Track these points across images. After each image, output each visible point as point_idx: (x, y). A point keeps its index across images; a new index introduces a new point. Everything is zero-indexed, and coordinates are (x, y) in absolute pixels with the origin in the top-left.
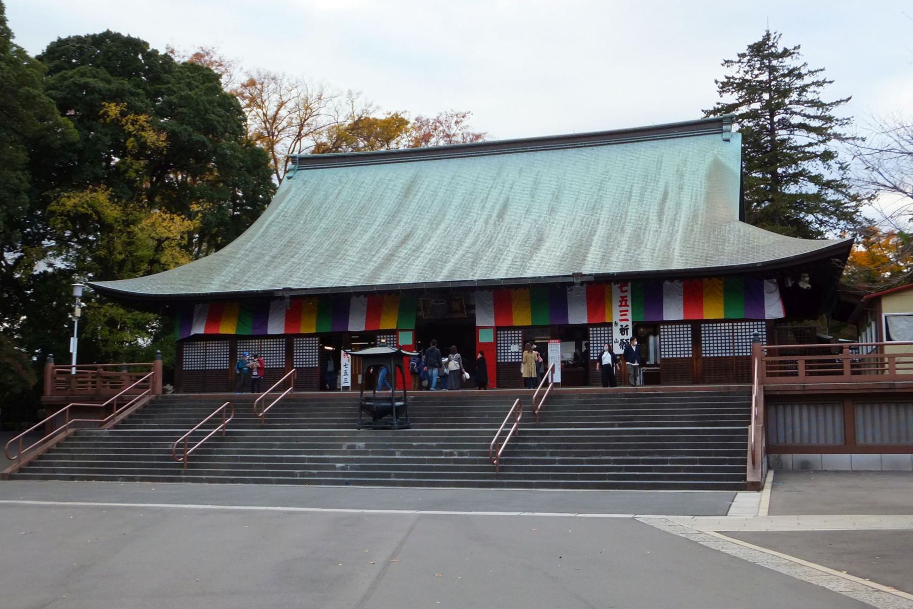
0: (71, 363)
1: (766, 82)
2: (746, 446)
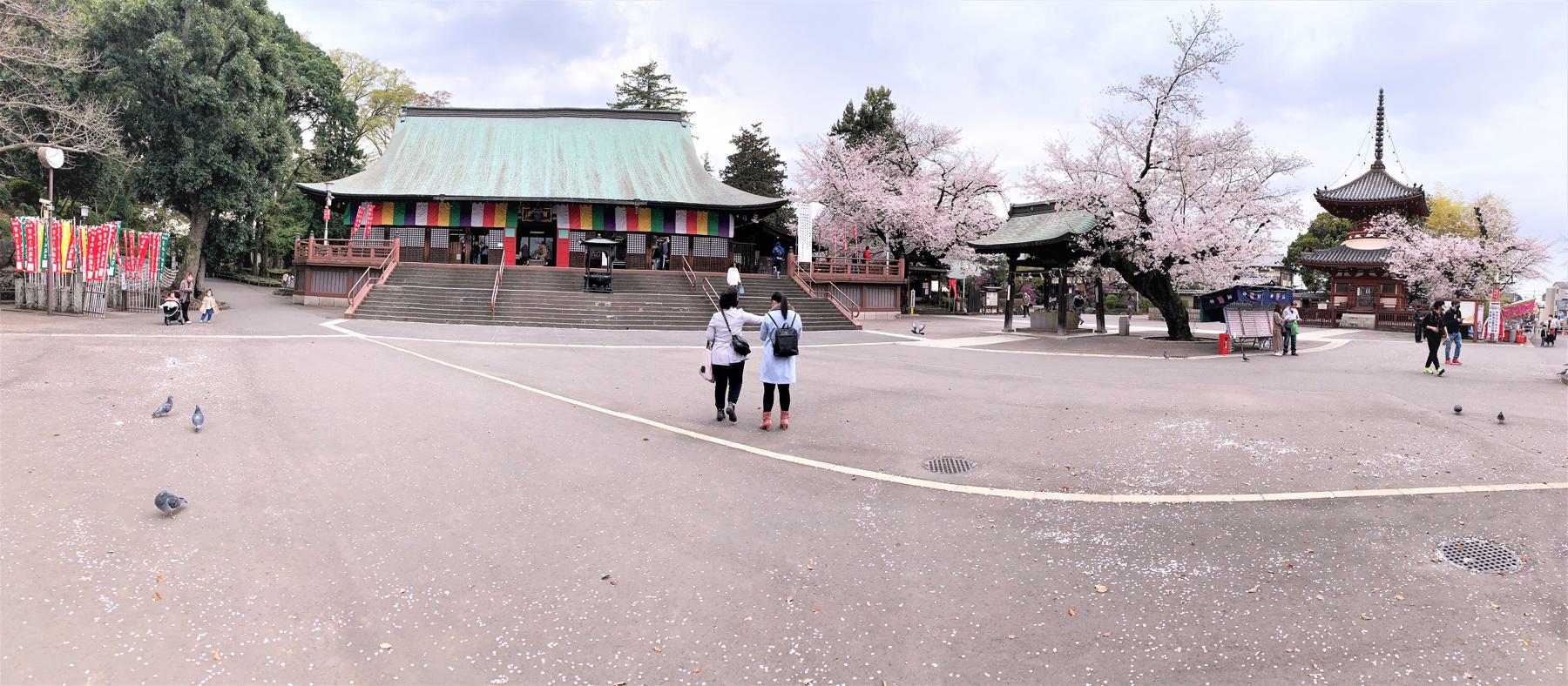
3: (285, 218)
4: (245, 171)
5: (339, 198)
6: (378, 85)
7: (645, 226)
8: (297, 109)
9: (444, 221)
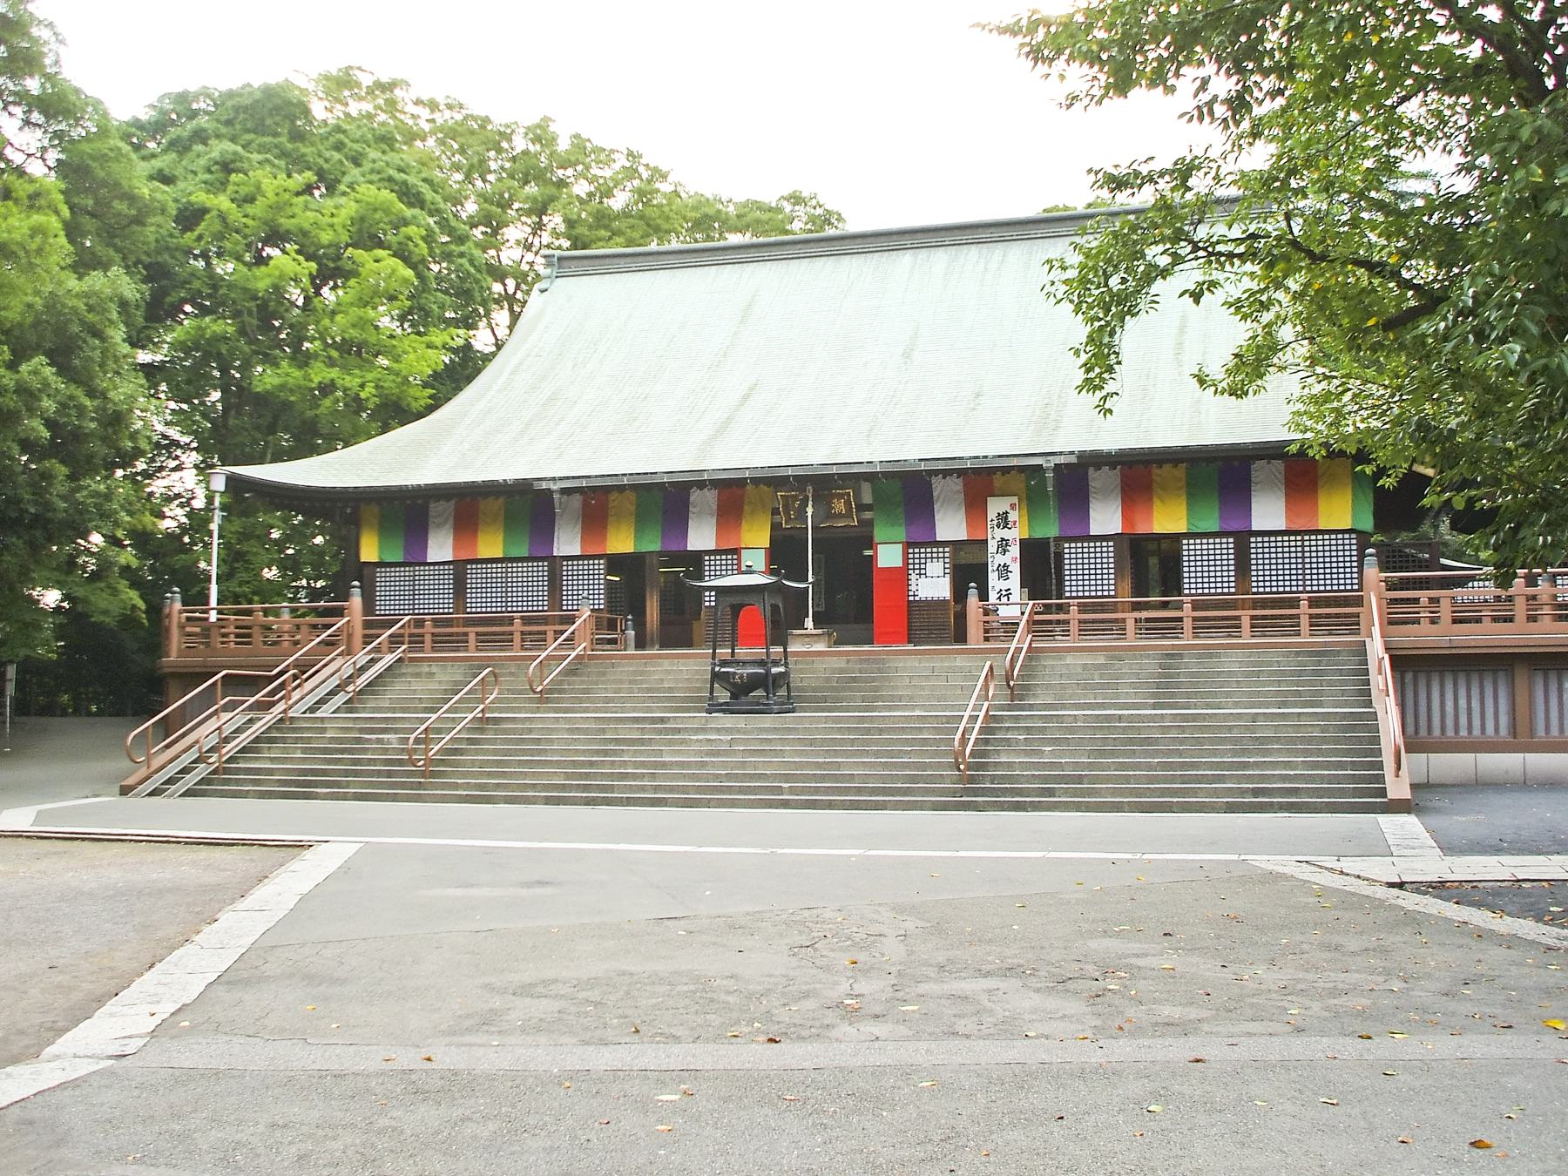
2: (1377, 740)
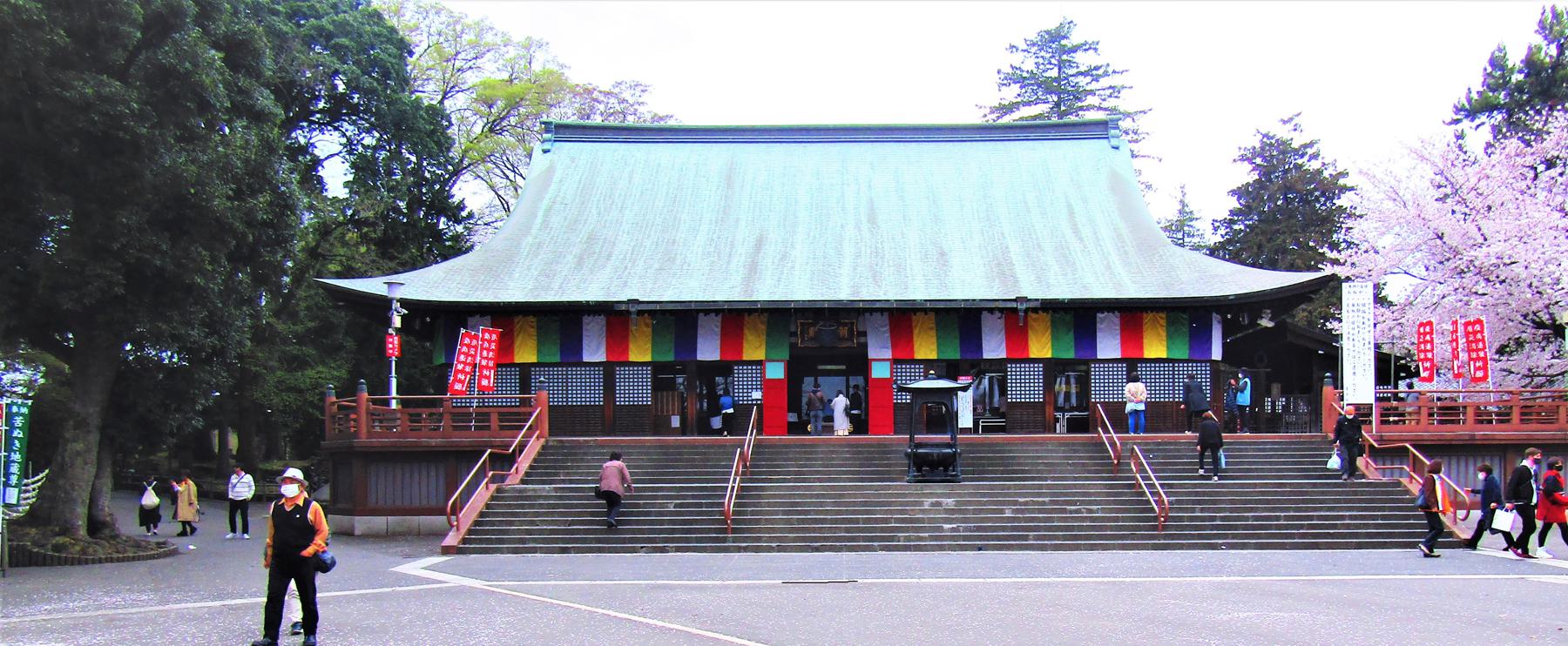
0: (389, 393)
1: (1055, 80)
3: (294, 350)
4: (210, 273)
5: (415, 308)
6: (491, 71)
7: (1041, 347)
8: (306, 115)
9: (640, 352)
